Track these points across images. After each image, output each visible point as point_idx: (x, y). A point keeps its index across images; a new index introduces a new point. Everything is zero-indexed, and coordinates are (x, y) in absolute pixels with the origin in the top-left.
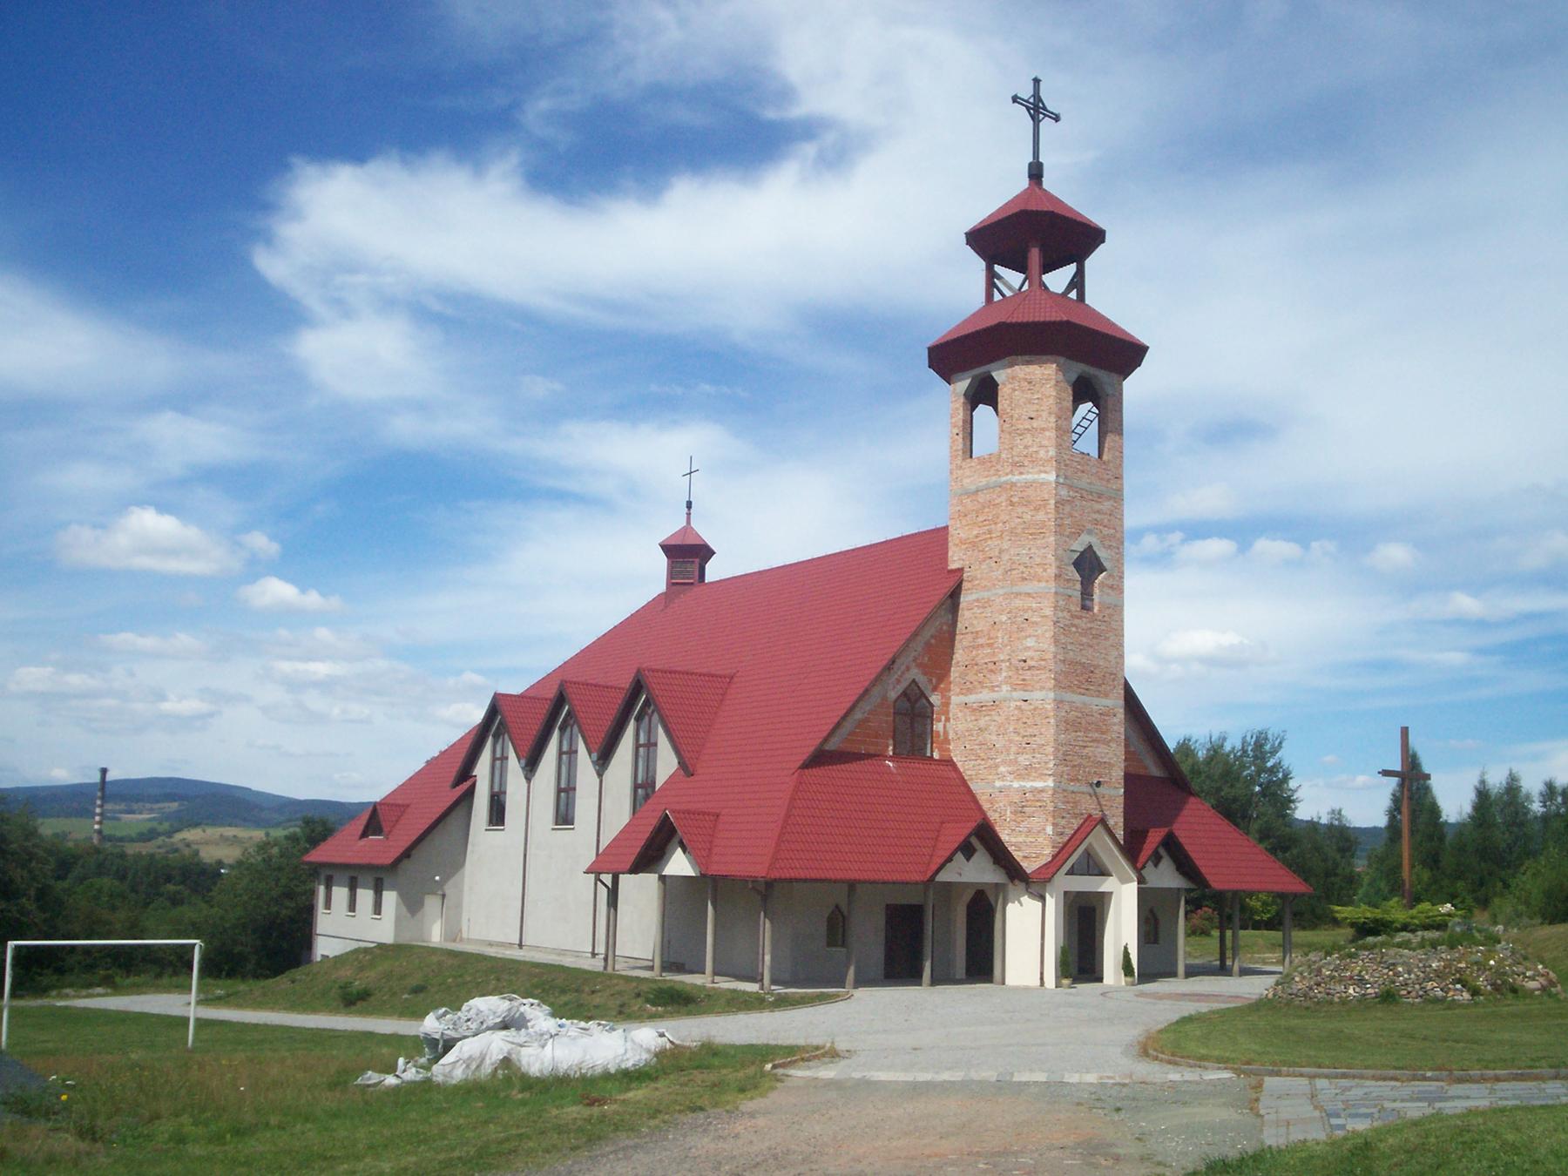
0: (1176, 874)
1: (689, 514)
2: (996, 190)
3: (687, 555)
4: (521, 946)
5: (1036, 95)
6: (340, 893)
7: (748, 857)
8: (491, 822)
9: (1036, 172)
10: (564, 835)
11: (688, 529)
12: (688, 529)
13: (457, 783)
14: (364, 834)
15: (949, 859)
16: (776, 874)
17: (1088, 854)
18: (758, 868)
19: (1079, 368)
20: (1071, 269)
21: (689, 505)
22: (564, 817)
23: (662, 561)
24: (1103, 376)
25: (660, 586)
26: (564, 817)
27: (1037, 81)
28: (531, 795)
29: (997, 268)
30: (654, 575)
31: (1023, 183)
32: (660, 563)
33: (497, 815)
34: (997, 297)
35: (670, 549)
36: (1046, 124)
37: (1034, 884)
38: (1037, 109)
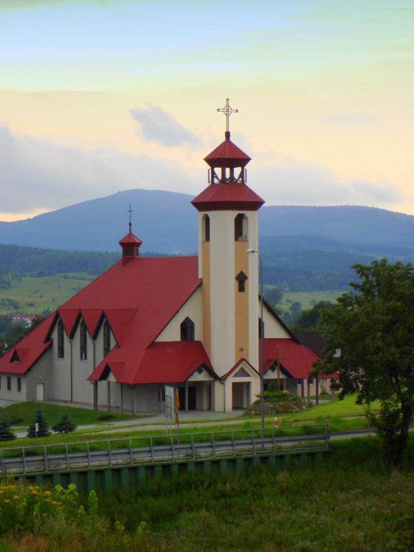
1: (130, 229)
3: (130, 246)
4: (72, 401)
5: (228, 106)
8: (59, 357)
9: (228, 134)
11: (130, 234)
12: (130, 234)
14: (12, 361)
15: (192, 375)
16: (136, 382)
17: (242, 369)
18: (131, 382)
19: (232, 215)
21: (130, 224)
28: (72, 346)
32: (120, 250)
33: (61, 354)
35: (123, 244)
36: (233, 116)
38: (228, 111)
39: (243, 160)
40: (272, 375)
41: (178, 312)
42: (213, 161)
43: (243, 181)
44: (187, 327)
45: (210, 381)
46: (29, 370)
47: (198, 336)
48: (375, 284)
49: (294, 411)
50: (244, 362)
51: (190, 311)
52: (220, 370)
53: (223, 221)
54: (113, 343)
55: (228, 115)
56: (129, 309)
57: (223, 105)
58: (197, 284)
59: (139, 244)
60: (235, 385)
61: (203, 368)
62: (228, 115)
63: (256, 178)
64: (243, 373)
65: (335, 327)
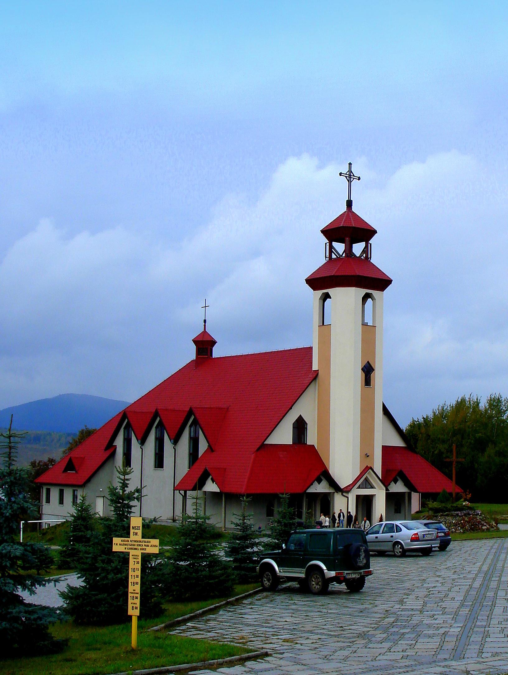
0: (405, 487)
1: (205, 326)
2: (334, 211)
3: (204, 344)
5: (350, 171)
6: (55, 493)
7: (239, 486)
9: (349, 204)
10: (159, 471)
11: (205, 332)
12: (205, 332)
13: (107, 449)
14: (65, 470)
17: (366, 480)
19: (363, 292)
20: (363, 244)
21: (205, 321)
22: (159, 463)
23: (194, 347)
24: (375, 293)
25: (194, 357)
26: (159, 463)
27: (350, 164)
29: (334, 244)
30: (190, 354)
31: (344, 209)
32: (193, 348)
34: (334, 256)
36: (355, 182)
37: (345, 491)
38: (350, 176)
39: (366, 233)
40: (398, 487)
41: (291, 408)
42: (332, 233)
43: (367, 258)
44: (300, 426)
45: (329, 494)
46: (89, 480)
47: (312, 439)
48: (13, 499)
49: (484, 527)
50: (370, 470)
51: (306, 408)
52: (344, 481)
53: (345, 298)
54: (203, 446)
55: (350, 182)
56: (210, 408)
57: (345, 170)
58: (311, 376)
59: (214, 343)
60: (358, 497)
61: (322, 478)
62: (350, 182)
63: (382, 255)
64: (367, 484)
65: (128, 490)
